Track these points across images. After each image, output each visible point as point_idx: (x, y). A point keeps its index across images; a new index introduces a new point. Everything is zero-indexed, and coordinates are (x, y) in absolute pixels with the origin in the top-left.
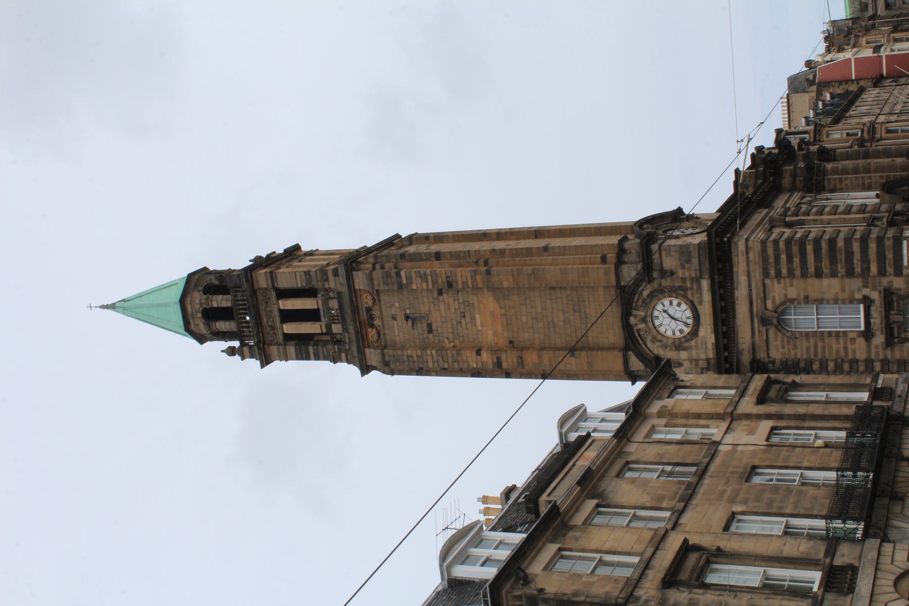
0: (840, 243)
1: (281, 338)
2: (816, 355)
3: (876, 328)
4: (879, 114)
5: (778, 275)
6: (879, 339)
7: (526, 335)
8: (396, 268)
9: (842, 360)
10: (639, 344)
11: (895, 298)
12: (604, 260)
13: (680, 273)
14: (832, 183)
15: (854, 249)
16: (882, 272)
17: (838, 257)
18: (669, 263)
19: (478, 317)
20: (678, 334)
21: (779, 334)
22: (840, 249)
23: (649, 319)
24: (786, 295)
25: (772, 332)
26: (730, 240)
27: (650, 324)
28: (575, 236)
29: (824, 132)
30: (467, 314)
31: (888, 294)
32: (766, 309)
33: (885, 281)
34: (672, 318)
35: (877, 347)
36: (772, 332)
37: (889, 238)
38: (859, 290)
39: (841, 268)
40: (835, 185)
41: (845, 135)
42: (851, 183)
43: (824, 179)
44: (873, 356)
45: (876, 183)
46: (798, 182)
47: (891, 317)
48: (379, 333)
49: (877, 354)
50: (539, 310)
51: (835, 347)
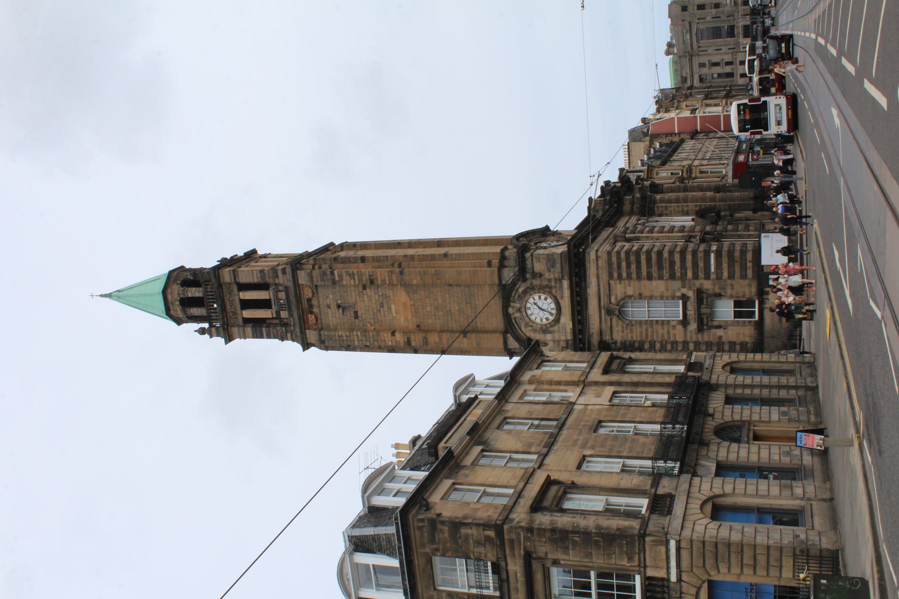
0: (666, 255)
1: (241, 322)
2: (647, 338)
5: (620, 277)
6: (693, 326)
7: (430, 321)
12: (489, 264)
13: (547, 275)
14: (660, 209)
16: (696, 276)
18: (539, 267)
19: (393, 306)
23: (523, 309)
27: (524, 313)
30: (385, 305)
31: (700, 293)
33: (697, 283)
35: (691, 332)
38: (679, 290)
44: (688, 339)
48: (317, 318)
49: (691, 337)
50: (440, 302)
51: (660, 333)
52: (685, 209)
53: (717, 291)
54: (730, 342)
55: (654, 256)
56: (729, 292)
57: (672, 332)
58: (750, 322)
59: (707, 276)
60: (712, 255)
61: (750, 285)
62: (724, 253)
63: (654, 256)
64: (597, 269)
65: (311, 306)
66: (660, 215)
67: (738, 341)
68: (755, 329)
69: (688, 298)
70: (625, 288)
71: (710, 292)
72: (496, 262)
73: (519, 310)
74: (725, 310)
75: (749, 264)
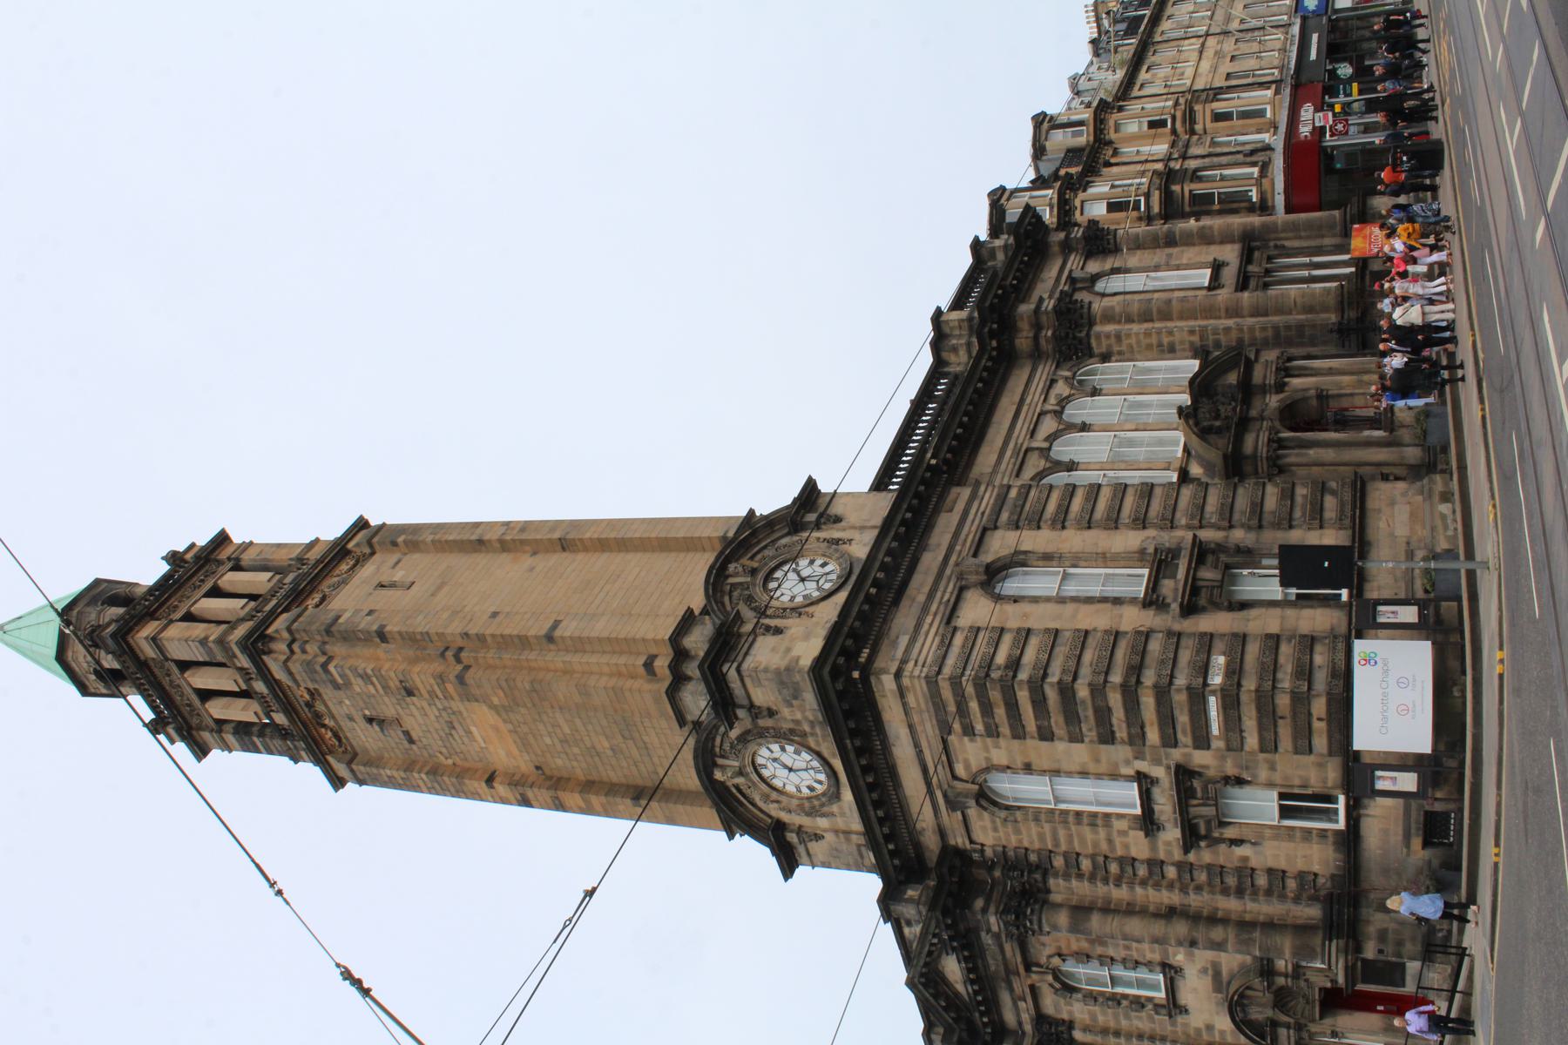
0: (1083, 692)
2: (1057, 844)
3: (1163, 818)
4: (1207, 35)
5: (969, 731)
6: (1172, 834)
7: (559, 762)
8: (324, 653)
9: (1106, 857)
10: (742, 804)
11: (1196, 784)
12: (649, 665)
13: (786, 712)
14: (1104, 342)
15: (1112, 703)
16: (1170, 741)
17: (1081, 714)
19: (473, 729)
20: (806, 791)
21: (986, 814)
22: (1083, 702)
24: (987, 759)
25: (973, 812)
26: (865, 678)
28: (627, 551)
29: (1111, 123)
30: (456, 724)
31: (1184, 775)
32: (955, 777)
33: (1176, 755)
34: (791, 770)
35: (1168, 844)
36: (973, 812)
37: (1179, 690)
38: (1127, 762)
39: (1089, 728)
40: (1109, 346)
41: (1145, 126)
42: (1138, 342)
43: (1088, 335)
44: (1162, 856)
45: (1182, 342)
46: (1043, 342)
47: (1193, 810)
48: (336, 735)
49: (1169, 853)
50: (567, 731)
51: (1088, 840)
52: (1166, 340)
53: (1230, 770)
54: (1270, 871)
55: (1052, 695)
56: (1263, 774)
57: (1118, 841)
58: (1323, 833)
59: (1202, 741)
60: (1212, 700)
61: (1321, 765)
62: (1244, 697)
63: (1052, 695)
64: (906, 714)
65: (318, 716)
66: (1105, 358)
67: (1292, 870)
68: (1336, 850)
69: (1154, 781)
70: (987, 749)
71: (1211, 773)
72: (662, 664)
73: (741, 772)
74: (1257, 806)
75: (1319, 726)
